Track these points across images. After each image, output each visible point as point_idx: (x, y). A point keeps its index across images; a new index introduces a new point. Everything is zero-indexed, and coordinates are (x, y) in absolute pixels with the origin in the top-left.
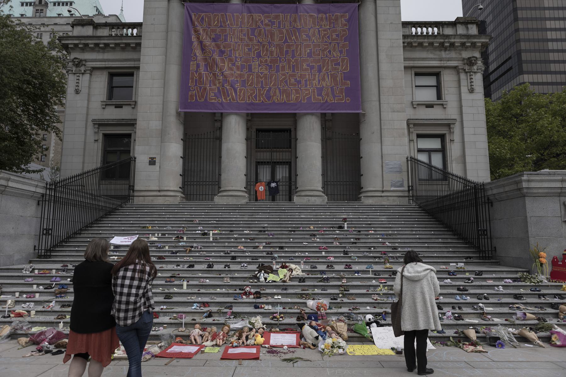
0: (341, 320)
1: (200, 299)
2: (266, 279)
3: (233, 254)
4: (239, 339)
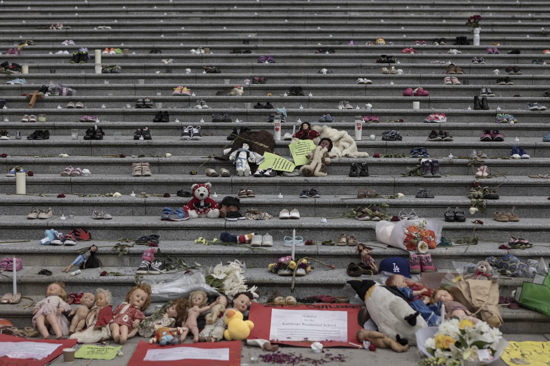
0: (480, 273)
1: (63, 219)
2: (254, 166)
3: (160, 107)
4: (178, 324)
